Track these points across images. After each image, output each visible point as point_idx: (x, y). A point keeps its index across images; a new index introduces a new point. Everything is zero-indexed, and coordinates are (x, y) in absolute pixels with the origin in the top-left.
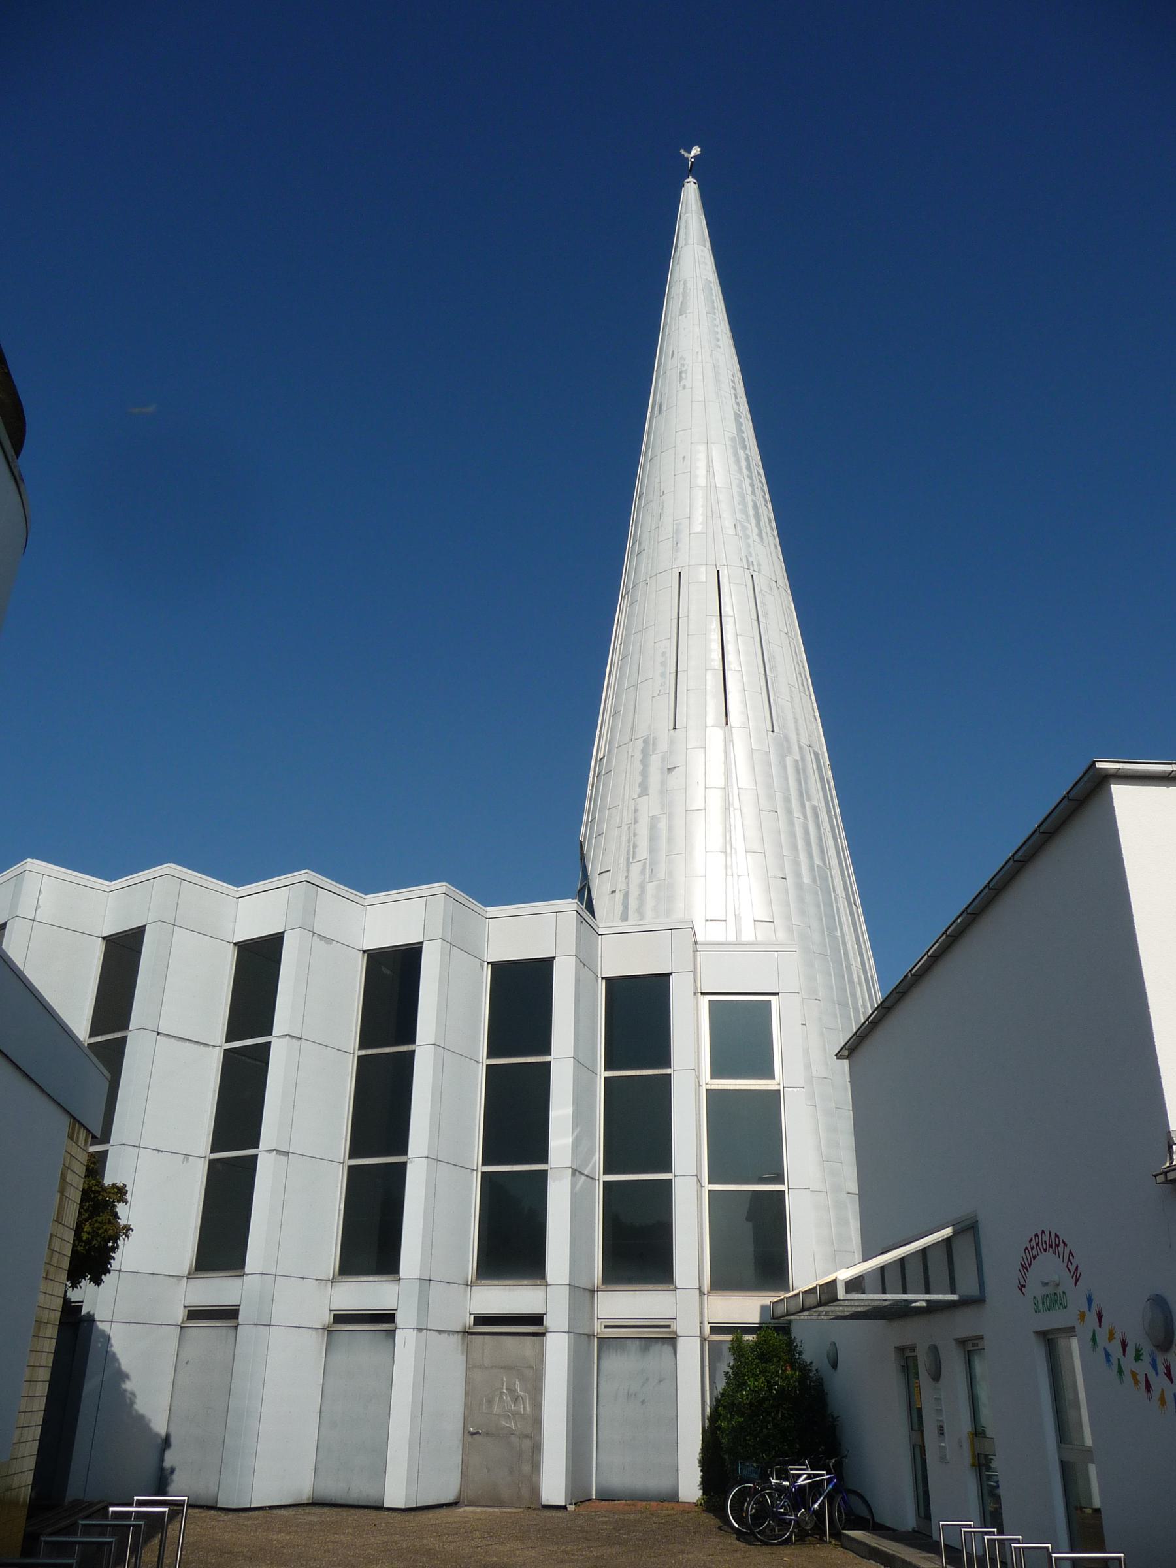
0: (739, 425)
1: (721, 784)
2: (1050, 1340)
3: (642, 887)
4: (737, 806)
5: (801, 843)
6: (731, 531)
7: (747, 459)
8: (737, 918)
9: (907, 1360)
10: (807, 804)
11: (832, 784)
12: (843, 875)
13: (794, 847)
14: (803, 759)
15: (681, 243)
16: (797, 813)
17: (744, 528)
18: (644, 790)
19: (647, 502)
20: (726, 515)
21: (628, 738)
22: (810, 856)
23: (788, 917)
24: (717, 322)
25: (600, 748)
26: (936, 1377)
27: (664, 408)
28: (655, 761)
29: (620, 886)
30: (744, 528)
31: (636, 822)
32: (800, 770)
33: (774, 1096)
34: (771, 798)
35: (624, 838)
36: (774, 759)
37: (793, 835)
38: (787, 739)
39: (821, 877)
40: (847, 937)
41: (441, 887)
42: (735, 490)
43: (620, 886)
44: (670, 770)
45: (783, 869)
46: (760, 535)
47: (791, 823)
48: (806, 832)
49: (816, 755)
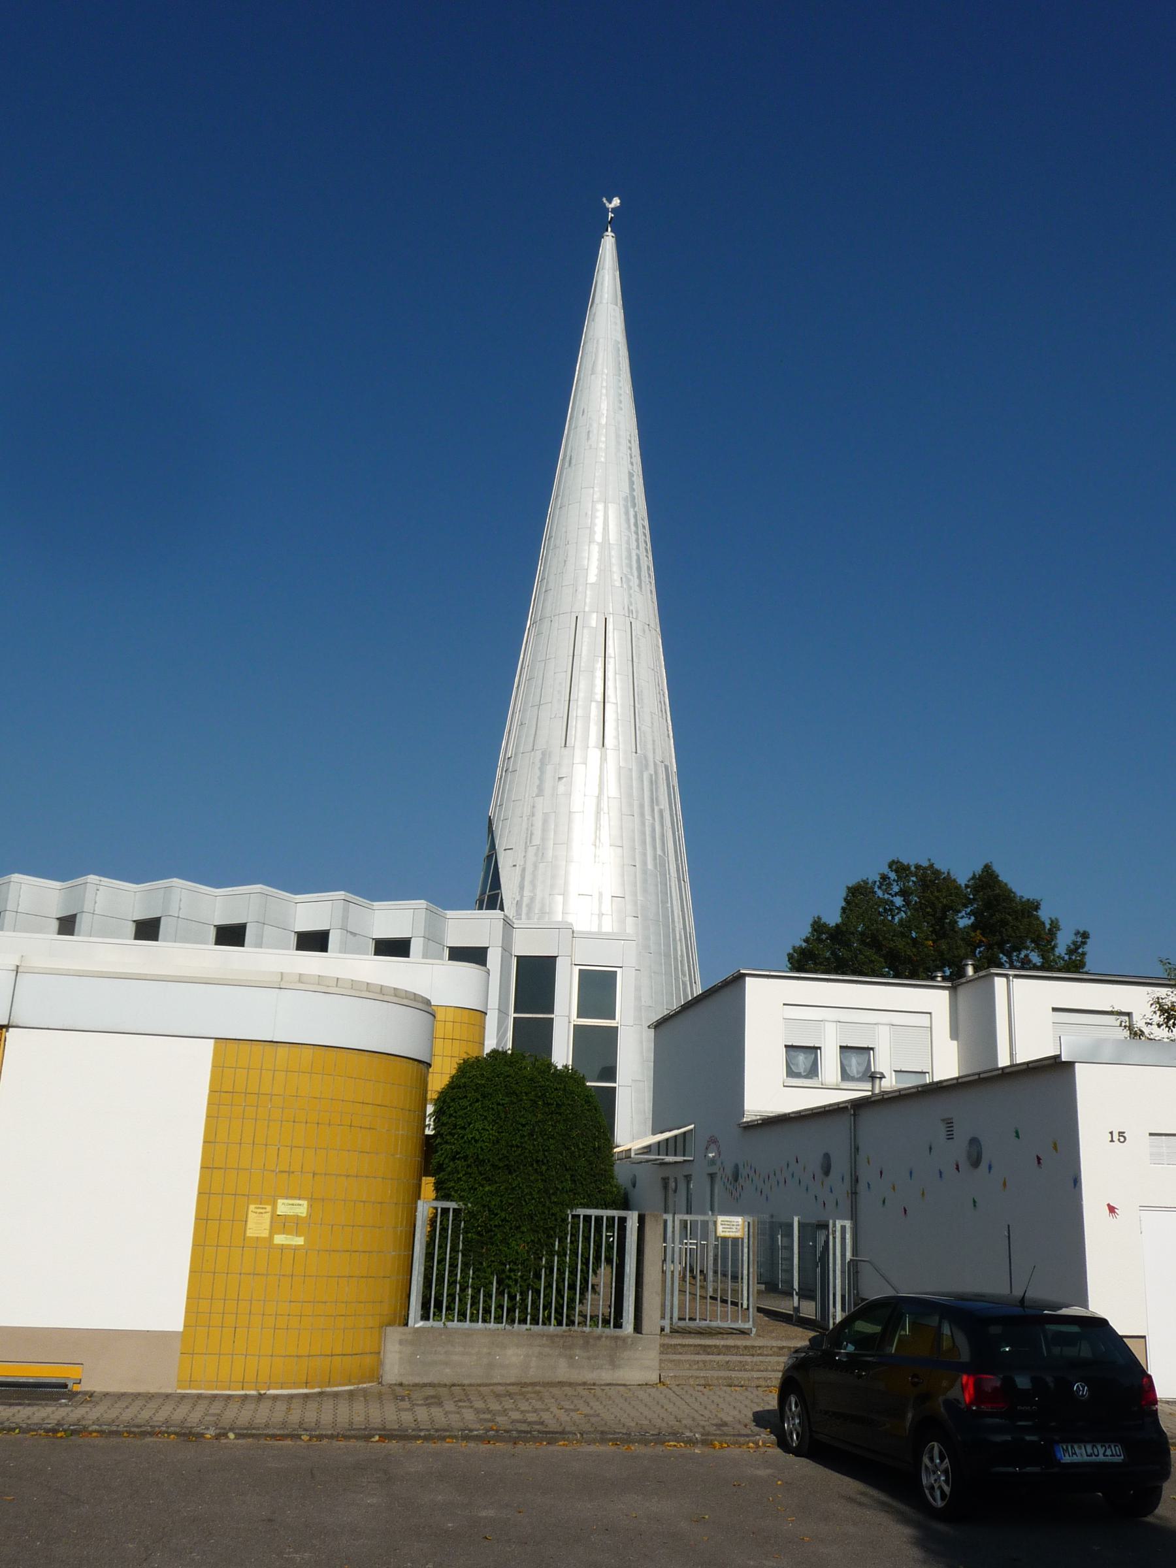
0: (632, 483)
2: (712, 1176)
3: (535, 866)
5: (648, 839)
6: (618, 584)
7: (636, 516)
8: (601, 894)
9: (665, 1181)
10: (656, 809)
11: (677, 788)
12: (677, 860)
13: (644, 842)
14: (656, 772)
15: (597, 300)
16: (648, 817)
17: (628, 580)
18: (540, 793)
20: (615, 569)
23: (635, 894)
24: (621, 384)
25: (508, 746)
26: (675, 1191)
27: (573, 462)
28: (549, 769)
30: (628, 580)
31: (533, 815)
32: (653, 783)
34: (631, 805)
35: (524, 826)
37: (644, 833)
39: (661, 863)
40: (675, 908)
41: (422, 903)
42: (624, 546)
43: (520, 862)
44: (560, 778)
45: (634, 859)
46: (640, 586)
47: (643, 824)
48: (654, 830)
49: (666, 768)
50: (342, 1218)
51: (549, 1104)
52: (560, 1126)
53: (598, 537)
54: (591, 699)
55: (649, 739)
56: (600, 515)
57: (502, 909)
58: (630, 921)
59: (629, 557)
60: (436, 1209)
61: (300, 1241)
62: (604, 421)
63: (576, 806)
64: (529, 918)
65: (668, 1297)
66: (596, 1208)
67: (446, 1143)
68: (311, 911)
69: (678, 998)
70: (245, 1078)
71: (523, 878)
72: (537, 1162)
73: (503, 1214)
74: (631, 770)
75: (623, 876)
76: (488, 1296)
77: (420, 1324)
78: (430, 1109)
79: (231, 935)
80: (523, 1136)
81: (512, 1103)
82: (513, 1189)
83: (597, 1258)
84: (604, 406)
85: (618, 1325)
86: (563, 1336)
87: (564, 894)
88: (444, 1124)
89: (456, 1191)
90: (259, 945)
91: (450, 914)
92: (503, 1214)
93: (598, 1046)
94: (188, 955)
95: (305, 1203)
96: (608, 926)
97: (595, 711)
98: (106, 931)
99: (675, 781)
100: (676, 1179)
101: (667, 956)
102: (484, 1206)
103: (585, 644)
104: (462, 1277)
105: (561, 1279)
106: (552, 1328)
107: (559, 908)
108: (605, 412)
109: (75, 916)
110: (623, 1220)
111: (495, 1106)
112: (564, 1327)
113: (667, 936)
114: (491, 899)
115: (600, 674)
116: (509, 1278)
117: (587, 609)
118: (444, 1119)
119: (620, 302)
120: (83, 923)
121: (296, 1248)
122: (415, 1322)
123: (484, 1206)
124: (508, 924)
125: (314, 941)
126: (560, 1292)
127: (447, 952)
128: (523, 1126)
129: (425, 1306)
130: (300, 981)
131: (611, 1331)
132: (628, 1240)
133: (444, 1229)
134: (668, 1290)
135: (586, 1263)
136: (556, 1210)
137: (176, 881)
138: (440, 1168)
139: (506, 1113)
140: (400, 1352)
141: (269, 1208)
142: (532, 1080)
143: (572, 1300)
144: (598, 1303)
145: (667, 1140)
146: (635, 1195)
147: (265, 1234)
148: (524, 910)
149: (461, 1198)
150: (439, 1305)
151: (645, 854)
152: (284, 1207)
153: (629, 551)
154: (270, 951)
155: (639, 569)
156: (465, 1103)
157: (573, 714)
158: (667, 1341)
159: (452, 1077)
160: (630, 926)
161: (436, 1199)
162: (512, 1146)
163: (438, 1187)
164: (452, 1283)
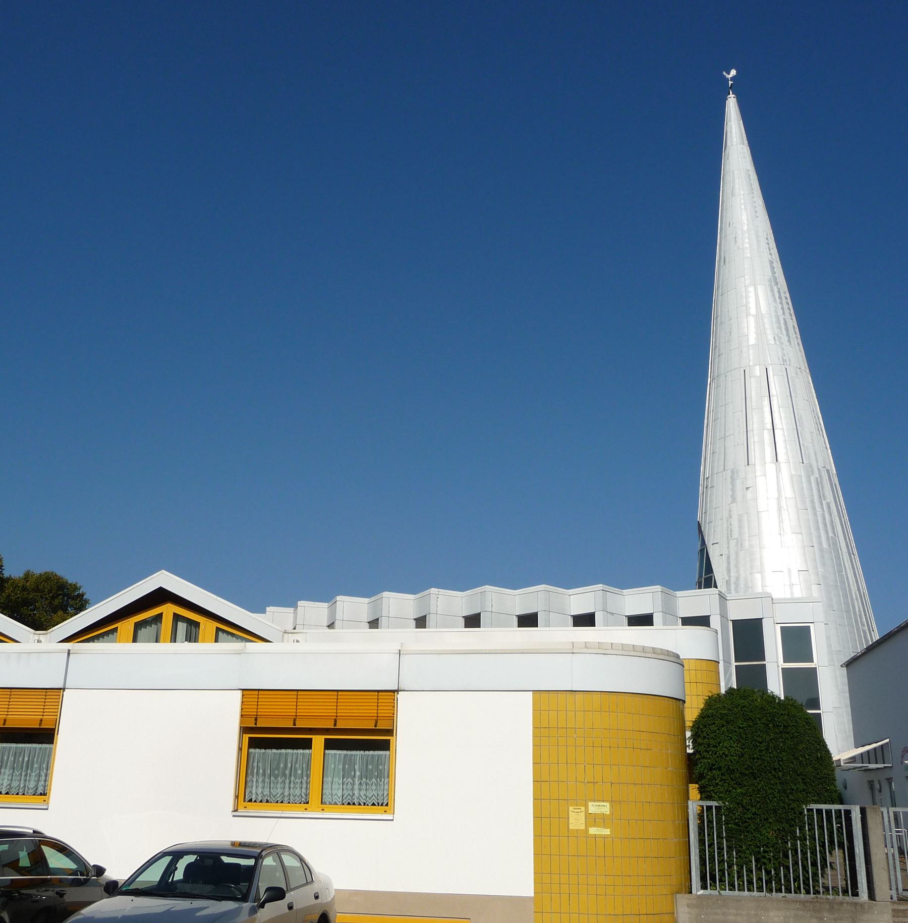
0: (773, 268)
1: (776, 496)
3: (737, 554)
4: (785, 507)
5: (821, 526)
6: (772, 342)
7: (779, 292)
8: (789, 570)
9: (871, 784)
10: (824, 502)
12: (845, 539)
13: (818, 529)
16: (818, 509)
17: (780, 338)
18: (734, 500)
19: (722, 323)
20: (769, 332)
21: (722, 468)
22: (827, 532)
23: (816, 568)
25: (705, 470)
26: (880, 791)
27: (727, 261)
28: (738, 483)
29: (725, 552)
30: (780, 338)
32: (819, 483)
33: (813, 671)
35: (725, 526)
36: (804, 480)
38: (811, 466)
39: (833, 543)
41: (658, 588)
42: (773, 314)
43: (725, 552)
45: (812, 541)
46: (789, 341)
49: (828, 471)
50: (641, 811)
51: (778, 726)
52: (789, 742)
53: (753, 311)
54: (763, 428)
55: (812, 452)
56: (752, 295)
57: (716, 587)
58: (815, 588)
59: (778, 322)
60: (702, 807)
61: (607, 832)
62: (745, 228)
63: (762, 504)
64: (736, 591)
65: (892, 873)
66: (825, 803)
67: (704, 758)
68: (581, 600)
69: (861, 644)
70: (559, 720)
71: (729, 563)
72: (775, 769)
73: (754, 810)
74: (800, 476)
75: (805, 554)
76: (750, 871)
77: (701, 892)
78: (688, 734)
79: (528, 620)
80: (761, 751)
81: (750, 726)
82: (759, 790)
83: (831, 842)
84: (744, 217)
85: (855, 894)
86: (811, 902)
87: (761, 572)
88: (700, 744)
89: (716, 793)
90: (548, 625)
91: (679, 593)
92: (754, 810)
93: (804, 682)
94: (502, 635)
95: (608, 804)
96: (798, 593)
97: (767, 436)
98: (446, 624)
99: (836, 480)
100: (879, 782)
101: (848, 611)
102: (738, 804)
103: (753, 389)
104: (728, 857)
105: (805, 858)
106: (802, 896)
107: (759, 583)
108: (745, 221)
109: (479, 614)
110: (848, 813)
111: (737, 729)
112: (812, 895)
113: (845, 596)
114: (707, 580)
115: (767, 409)
116: (764, 857)
117: (751, 364)
118: (700, 740)
119: (746, 142)
120: (431, 620)
121: (604, 837)
122: (698, 891)
123: (738, 804)
124: (722, 597)
125: (585, 620)
126: (805, 868)
127: (680, 621)
128: (761, 743)
129: (703, 878)
130: (586, 647)
131: (850, 898)
132: (854, 828)
133: (710, 822)
134: (891, 868)
135: (823, 845)
136: (794, 805)
137: (488, 588)
138: (701, 777)
139: (745, 734)
140: (689, 913)
141: (583, 809)
142: (762, 708)
143: (815, 874)
144: (835, 876)
145: (862, 754)
146: (847, 794)
147: (583, 827)
148: (733, 587)
149: (720, 798)
150: (713, 878)
151: (819, 537)
152: (594, 808)
153: (777, 317)
154: (555, 628)
155: (787, 329)
156: (713, 728)
157: (751, 441)
158: (896, 907)
159: (702, 710)
160: (816, 592)
161: (701, 799)
162: (754, 758)
163: (702, 790)
164: (721, 862)
